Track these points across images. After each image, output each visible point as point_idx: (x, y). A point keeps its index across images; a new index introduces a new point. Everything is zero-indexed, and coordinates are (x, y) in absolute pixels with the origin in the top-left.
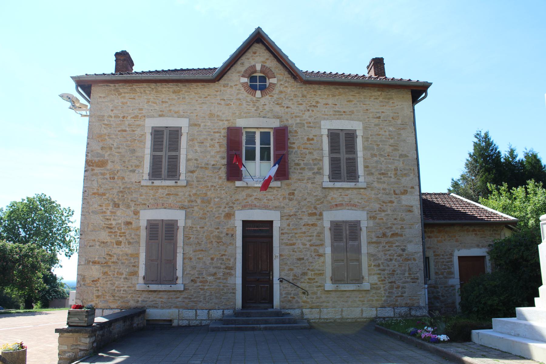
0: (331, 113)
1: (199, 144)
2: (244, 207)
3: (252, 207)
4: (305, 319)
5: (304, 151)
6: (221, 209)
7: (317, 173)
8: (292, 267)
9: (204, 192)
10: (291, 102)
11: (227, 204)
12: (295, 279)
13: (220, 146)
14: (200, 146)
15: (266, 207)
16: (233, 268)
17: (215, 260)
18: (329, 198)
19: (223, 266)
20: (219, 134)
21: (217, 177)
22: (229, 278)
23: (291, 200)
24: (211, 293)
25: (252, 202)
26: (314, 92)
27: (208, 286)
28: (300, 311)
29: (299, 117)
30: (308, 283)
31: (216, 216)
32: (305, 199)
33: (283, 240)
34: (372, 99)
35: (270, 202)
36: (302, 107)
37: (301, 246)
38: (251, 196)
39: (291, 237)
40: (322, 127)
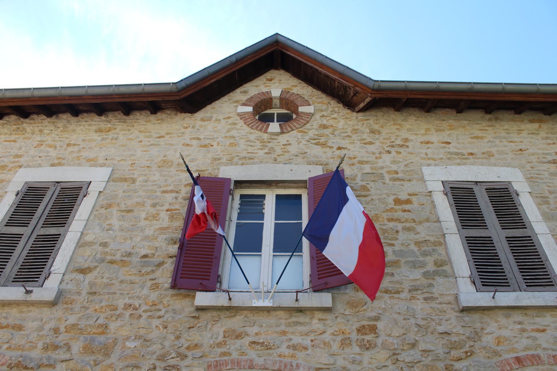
0: (442, 156)
1: (120, 214)
5: (391, 224)
7: (436, 273)
9: (101, 321)
10: (347, 141)
13: (172, 218)
14: (122, 218)
18: (488, 340)
20: (174, 195)
21: (149, 283)
23: (367, 347)
25: (243, 354)
26: (394, 124)
29: (367, 162)
34: (524, 134)
35: (301, 355)
36: (371, 148)
38: (239, 336)
40: (426, 178)
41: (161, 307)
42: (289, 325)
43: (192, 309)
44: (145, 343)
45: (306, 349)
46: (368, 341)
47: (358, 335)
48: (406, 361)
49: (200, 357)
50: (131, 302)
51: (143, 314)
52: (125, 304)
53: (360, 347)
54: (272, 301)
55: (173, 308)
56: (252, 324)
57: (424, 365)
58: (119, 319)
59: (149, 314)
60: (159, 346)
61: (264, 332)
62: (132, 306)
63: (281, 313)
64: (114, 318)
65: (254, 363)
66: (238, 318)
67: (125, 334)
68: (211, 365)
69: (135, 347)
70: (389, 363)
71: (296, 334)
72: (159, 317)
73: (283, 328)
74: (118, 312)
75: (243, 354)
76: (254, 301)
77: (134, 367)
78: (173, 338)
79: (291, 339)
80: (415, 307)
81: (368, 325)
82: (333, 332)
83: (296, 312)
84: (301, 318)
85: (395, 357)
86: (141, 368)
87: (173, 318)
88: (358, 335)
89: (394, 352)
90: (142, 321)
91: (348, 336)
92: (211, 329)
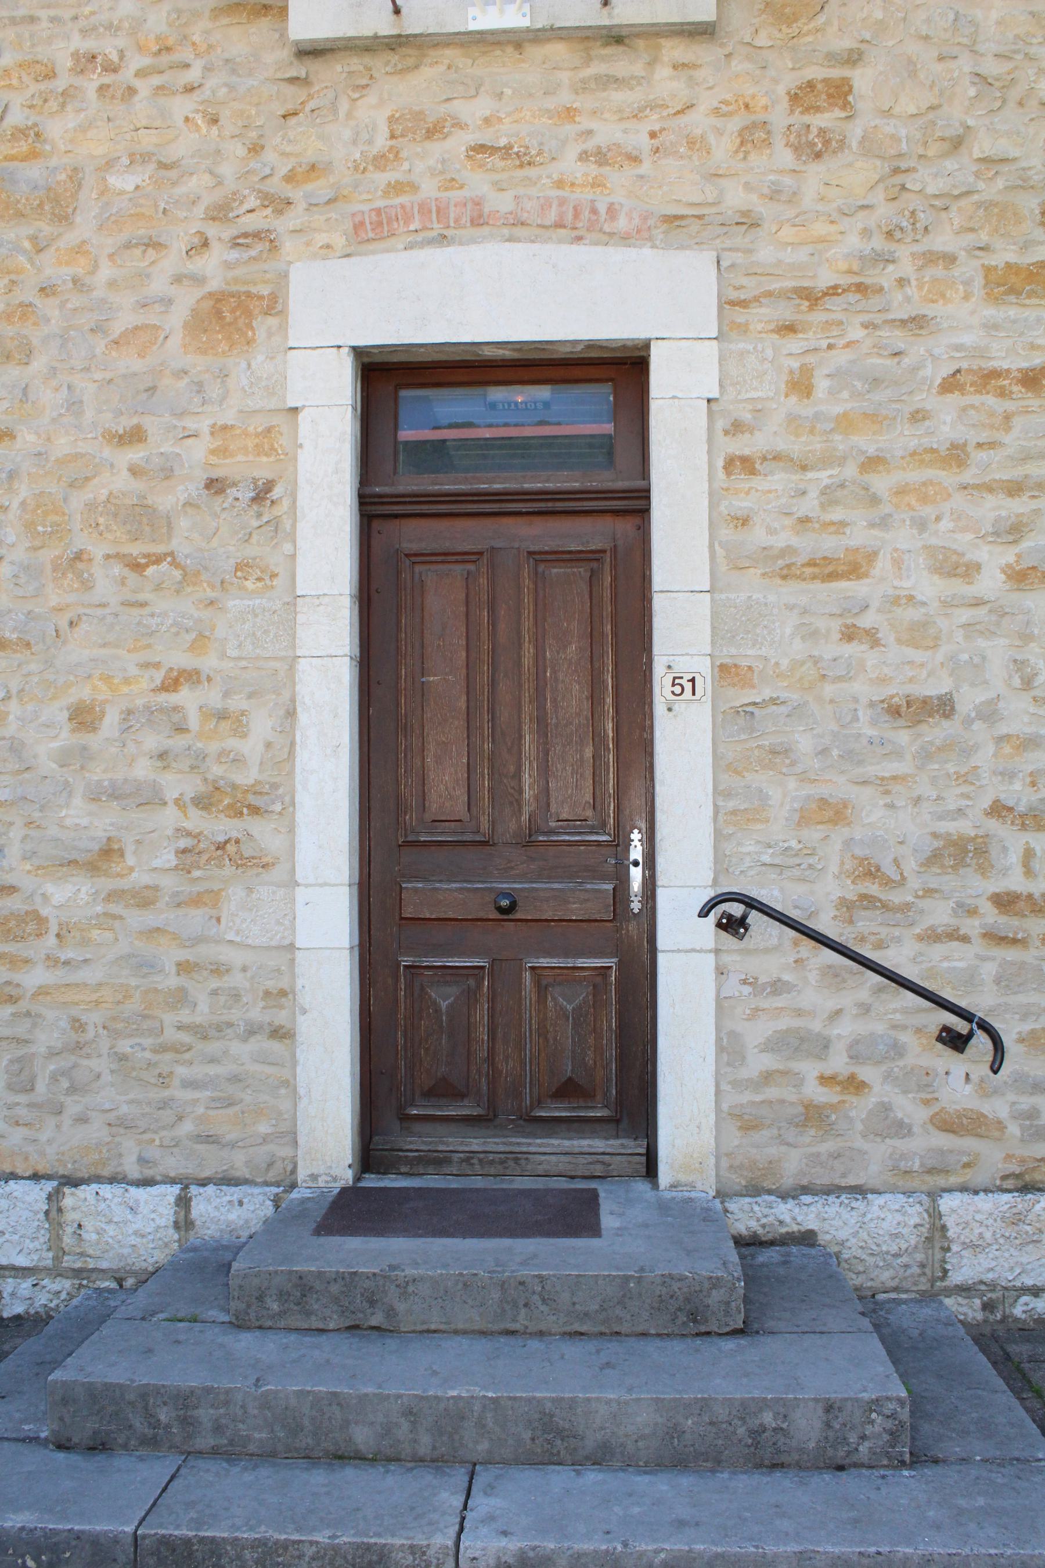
2: (372, 231)
3: (448, 222)
4: (964, 1290)
6: (171, 262)
8: (838, 786)
11: (220, 213)
12: (867, 901)
15: (578, 223)
16: (257, 801)
17: (111, 720)
19: (177, 784)
22: (236, 893)
23: (815, 149)
24: (78, 1025)
25: (452, 184)
27: (52, 961)
28: (915, 1213)
30: (996, 938)
31: (123, 321)
32: (957, 144)
33: (743, 521)
35: (619, 181)
37: (928, 587)
38: (435, 131)
39: (829, 496)
41: (185, 54)
42: (582, 87)
43: (285, 54)
44: (163, 173)
45: (635, 159)
46: (822, 131)
47: (792, 111)
48: (931, 190)
49: (330, 202)
50: (89, 45)
51: (137, 83)
52: (76, 55)
53: (797, 149)
54: (526, 9)
55: (226, 56)
56: (473, 92)
57: (979, 205)
58: (69, 108)
59: (156, 80)
60: (207, 179)
61: (509, 115)
62: (99, 59)
63: (558, 50)
64: (53, 105)
65: (486, 210)
66: (427, 72)
67: (99, 151)
68: (362, 223)
69: (137, 187)
70: (878, 197)
71: (606, 115)
72: (190, 89)
73: (565, 97)
74: (61, 84)
75: (452, 184)
76: (472, 12)
77: (147, 245)
78: (241, 151)
79: (590, 132)
80: (979, 14)
81: (825, 81)
82: (715, 104)
83: (607, 44)
84: (622, 63)
85: (898, 179)
86: (166, 247)
87: (231, 88)
88: (792, 111)
89: (896, 164)
90: (142, 107)
91: (760, 117)
92: (349, 115)
